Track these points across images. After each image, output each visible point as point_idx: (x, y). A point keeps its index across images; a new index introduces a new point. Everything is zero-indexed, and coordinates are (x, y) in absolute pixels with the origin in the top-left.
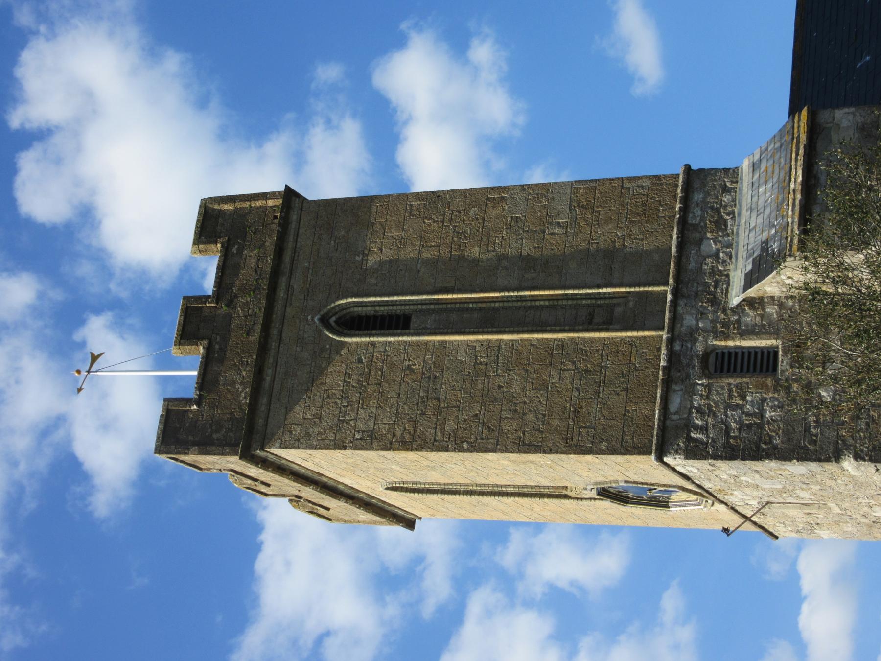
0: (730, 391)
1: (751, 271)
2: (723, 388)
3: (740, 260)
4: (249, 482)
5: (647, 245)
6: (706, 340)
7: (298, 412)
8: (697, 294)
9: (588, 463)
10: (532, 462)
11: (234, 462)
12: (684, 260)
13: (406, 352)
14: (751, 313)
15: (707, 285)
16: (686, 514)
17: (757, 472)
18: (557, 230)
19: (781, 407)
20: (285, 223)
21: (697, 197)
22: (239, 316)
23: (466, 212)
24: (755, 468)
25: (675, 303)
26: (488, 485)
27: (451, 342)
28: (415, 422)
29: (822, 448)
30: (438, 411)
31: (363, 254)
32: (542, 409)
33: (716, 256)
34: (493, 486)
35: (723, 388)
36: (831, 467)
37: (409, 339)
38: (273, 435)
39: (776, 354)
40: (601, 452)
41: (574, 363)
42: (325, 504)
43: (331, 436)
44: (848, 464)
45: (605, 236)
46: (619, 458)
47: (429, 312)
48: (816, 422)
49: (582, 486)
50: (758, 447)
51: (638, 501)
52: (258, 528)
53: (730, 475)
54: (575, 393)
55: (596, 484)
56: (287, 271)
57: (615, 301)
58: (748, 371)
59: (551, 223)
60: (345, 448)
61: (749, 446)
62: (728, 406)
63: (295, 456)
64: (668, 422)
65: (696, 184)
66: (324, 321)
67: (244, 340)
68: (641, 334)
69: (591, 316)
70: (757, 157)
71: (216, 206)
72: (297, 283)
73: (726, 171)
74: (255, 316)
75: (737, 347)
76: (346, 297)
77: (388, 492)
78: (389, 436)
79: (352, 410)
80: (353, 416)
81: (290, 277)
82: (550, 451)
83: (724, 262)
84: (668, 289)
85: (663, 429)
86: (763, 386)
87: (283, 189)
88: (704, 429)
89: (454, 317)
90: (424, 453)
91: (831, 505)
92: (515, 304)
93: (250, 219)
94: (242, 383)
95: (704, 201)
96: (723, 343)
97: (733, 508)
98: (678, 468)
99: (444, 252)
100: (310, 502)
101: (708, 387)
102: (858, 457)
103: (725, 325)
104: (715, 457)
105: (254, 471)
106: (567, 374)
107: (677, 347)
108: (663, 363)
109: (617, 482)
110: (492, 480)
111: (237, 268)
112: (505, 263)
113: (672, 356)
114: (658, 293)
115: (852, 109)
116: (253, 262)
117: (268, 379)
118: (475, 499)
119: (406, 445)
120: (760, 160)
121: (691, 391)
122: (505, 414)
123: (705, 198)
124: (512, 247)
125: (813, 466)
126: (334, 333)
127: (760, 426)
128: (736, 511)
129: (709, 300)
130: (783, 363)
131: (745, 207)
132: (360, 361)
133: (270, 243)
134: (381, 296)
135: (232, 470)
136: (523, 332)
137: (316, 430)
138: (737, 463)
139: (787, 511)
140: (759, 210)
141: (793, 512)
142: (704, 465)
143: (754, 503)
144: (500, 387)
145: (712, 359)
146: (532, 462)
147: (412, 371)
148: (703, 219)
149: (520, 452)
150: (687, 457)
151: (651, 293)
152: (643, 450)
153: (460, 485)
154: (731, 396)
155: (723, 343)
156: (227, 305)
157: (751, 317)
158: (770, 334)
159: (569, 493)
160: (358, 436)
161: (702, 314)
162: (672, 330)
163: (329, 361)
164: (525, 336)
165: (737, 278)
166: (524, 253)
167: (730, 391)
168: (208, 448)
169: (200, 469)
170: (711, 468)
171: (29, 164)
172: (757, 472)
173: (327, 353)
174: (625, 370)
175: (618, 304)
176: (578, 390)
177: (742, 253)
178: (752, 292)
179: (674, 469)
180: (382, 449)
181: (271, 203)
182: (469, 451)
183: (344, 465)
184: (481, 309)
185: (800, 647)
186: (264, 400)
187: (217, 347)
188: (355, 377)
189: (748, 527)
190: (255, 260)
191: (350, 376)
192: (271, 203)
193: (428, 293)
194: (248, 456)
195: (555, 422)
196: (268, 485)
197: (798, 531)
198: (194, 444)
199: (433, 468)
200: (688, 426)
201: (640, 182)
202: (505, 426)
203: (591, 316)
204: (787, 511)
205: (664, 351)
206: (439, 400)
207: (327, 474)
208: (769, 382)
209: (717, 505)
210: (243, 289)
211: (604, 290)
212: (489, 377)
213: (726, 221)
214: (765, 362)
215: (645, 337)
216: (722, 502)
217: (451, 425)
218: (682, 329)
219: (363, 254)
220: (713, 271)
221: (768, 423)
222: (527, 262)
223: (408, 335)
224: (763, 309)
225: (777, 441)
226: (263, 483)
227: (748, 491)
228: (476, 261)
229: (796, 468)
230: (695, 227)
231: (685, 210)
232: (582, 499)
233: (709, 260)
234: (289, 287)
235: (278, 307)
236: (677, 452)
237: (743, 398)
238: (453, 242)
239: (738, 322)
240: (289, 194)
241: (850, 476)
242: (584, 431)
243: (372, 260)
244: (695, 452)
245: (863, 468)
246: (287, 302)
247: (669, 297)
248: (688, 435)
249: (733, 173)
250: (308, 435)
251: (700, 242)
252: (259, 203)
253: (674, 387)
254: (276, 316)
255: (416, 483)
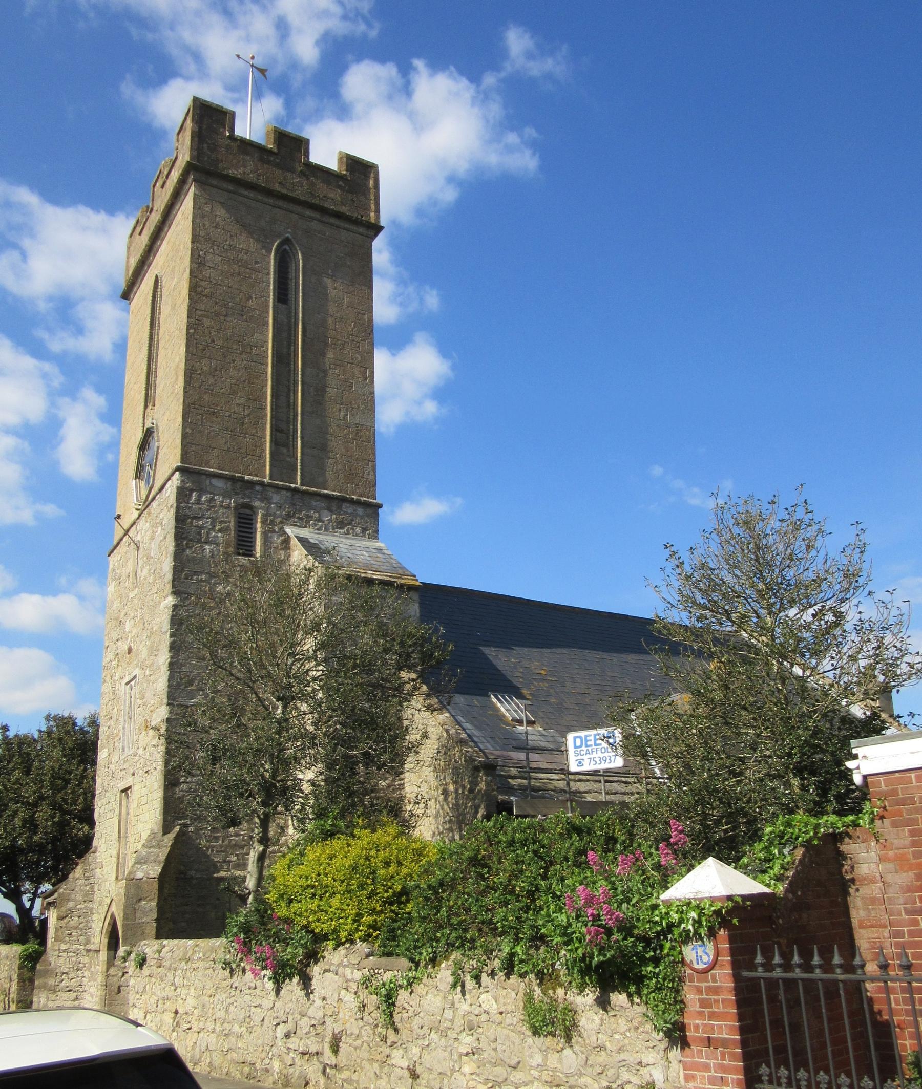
0: (225, 522)
1: (309, 542)
2: (227, 517)
3: (317, 536)
4: (166, 173)
5: (329, 474)
6: (262, 508)
7: (221, 212)
8: (294, 505)
9: (175, 419)
10: (176, 379)
11: (184, 157)
12: (318, 498)
13: (262, 297)
14: (279, 541)
15: (300, 512)
16: (129, 494)
17: (165, 538)
18: (342, 414)
19: (212, 557)
20: (357, 222)
21: (360, 511)
22: (293, 179)
23: (357, 352)
24: (168, 536)
25: (289, 489)
26: (158, 349)
27: (268, 330)
28: (210, 297)
29: (183, 582)
30: (217, 314)
31: (333, 276)
32: (217, 389)
33: (319, 520)
34: (157, 353)
35: (227, 517)
36: (169, 588)
37: (271, 300)
38: (204, 190)
39: (251, 556)
40: (184, 428)
41: (249, 415)
42: (144, 232)
43: (202, 233)
44: (171, 600)
45: (336, 445)
46: (178, 441)
47: (289, 317)
48: (201, 580)
49: (155, 417)
50: (184, 538)
51: (140, 458)
52: (111, 212)
53: (162, 519)
54: (227, 414)
55: (157, 426)
56: (324, 219)
57: (291, 448)
58: (239, 536)
59: (347, 409)
60: (193, 242)
61: (185, 532)
62: (214, 520)
63: (187, 205)
64: (204, 477)
65: (369, 511)
66: (287, 241)
67: (274, 179)
68: (268, 464)
69: (281, 431)
70: (386, 552)
71: (372, 175)
72: (315, 225)
73: (377, 532)
74: (293, 191)
75: (256, 529)
76: (303, 259)
77: (154, 278)
78: (201, 277)
79: (221, 252)
80: (217, 252)
81: (319, 220)
82: (185, 392)
83: (316, 525)
84: (298, 485)
85: (200, 473)
86: (228, 545)
87: (382, 224)
88: (198, 501)
89: (285, 335)
90: (187, 301)
91: (136, 592)
92: (292, 379)
93: (362, 198)
94: (244, 173)
95: (357, 515)
96: (259, 520)
97: (134, 523)
98: (170, 482)
99: (332, 333)
100: (147, 220)
101: (228, 507)
102: (175, 607)
103: (272, 522)
104: (178, 508)
105: (175, 175)
106: (241, 409)
107: (258, 488)
108: (246, 477)
109: (158, 441)
110: (161, 352)
111: (328, 183)
112: (321, 375)
113: (252, 484)
114: (296, 479)
115: (418, 615)
116: (332, 195)
117: (246, 193)
118: (147, 341)
119: (193, 288)
120: (384, 554)
121: (226, 495)
122: (214, 362)
123: (359, 515)
124: (332, 381)
125: (169, 576)
126: (277, 246)
127: (199, 541)
128: (132, 526)
129: (289, 512)
130: (244, 560)
131: (353, 542)
132: (256, 263)
133: (344, 209)
134: (303, 284)
135: (176, 158)
136: (272, 382)
137: (207, 223)
138: (173, 523)
139: (131, 560)
140: (354, 550)
141: (130, 566)
142: (172, 500)
143: (139, 538)
144: (234, 361)
145: (248, 511)
146: (176, 379)
147: (248, 300)
148: (345, 513)
149: (186, 370)
150: (178, 488)
151: (296, 474)
152: (184, 457)
153: (159, 330)
154: (221, 522)
155: (259, 520)
156: (301, 171)
157: (277, 540)
158: (265, 552)
159: (150, 407)
160: (201, 253)
161: (280, 508)
162: (270, 485)
163: (258, 240)
164: (269, 383)
165: (305, 533)
166: (328, 389)
167: (225, 522)
168: (196, 139)
169: (178, 134)
170: (169, 505)
171: (389, 71)
172: (165, 538)
173: (264, 241)
174: (243, 451)
175: (289, 451)
176: (230, 416)
177: (321, 537)
178: (294, 542)
179: (169, 479)
180: (191, 270)
181: (372, 215)
182: (188, 334)
183: (177, 243)
184: (289, 354)
185: (9, 594)
186: (231, 187)
187: (272, 159)
188: (245, 257)
189: (119, 533)
190: (333, 198)
191: (246, 254)
192: (372, 215)
193: (303, 318)
194: (189, 168)
195: (206, 397)
196: (162, 187)
197: (114, 570)
198: (200, 128)
199: (173, 308)
200: (201, 491)
201: (371, 473)
202: (205, 362)
203: (281, 431)
204: (131, 560)
205: (255, 479)
206: (226, 316)
207: (171, 231)
208: (231, 550)
209: (136, 514)
210: (313, 185)
211: (299, 442)
212: (241, 354)
213: (343, 528)
214: (244, 544)
215: (265, 466)
216: (140, 515)
217: (207, 322)
218: (270, 492)
219: (333, 276)
220: (309, 517)
221: (202, 547)
222: (321, 390)
223: (274, 300)
224: (282, 549)
225: (188, 552)
226: (164, 183)
227: (149, 533)
228: (323, 354)
229: (167, 565)
230: (340, 508)
231: (352, 501)
232: (144, 417)
233: (317, 515)
234: (312, 219)
235: (299, 209)
236: (182, 481)
237: (220, 531)
238: (338, 340)
239: (274, 531)
240: (377, 229)
241: (160, 603)
242: (199, 417)
243: (328, 282)
244: (182, 494)
245: (166, 610)
246: (301, 215)
247: (293, 486)
248: (194, 490)
249: (375, 536)
250: (203, 216)
251: (329, 510)
252: (373, 206)
253: (230, 483)
254: (291, 206)
255: (161, 296)
